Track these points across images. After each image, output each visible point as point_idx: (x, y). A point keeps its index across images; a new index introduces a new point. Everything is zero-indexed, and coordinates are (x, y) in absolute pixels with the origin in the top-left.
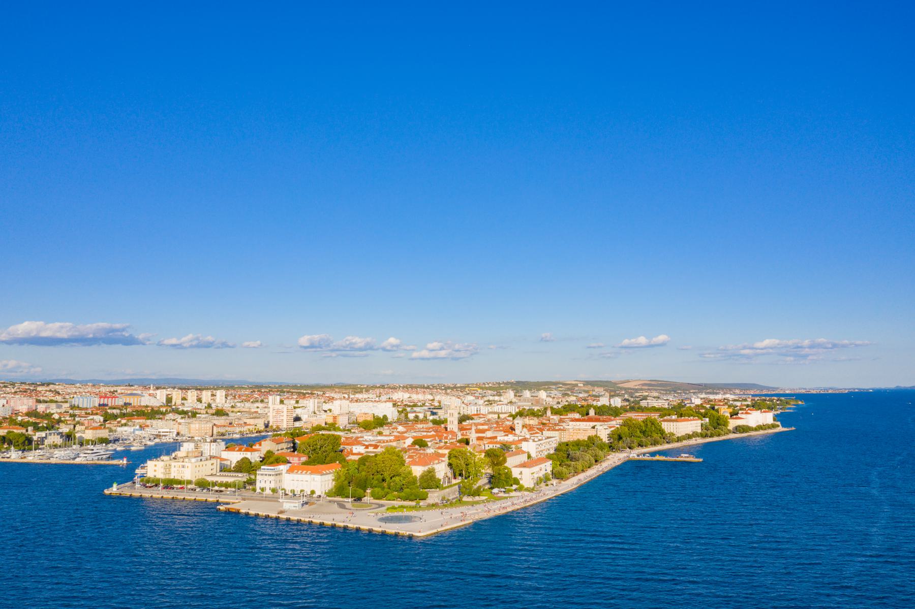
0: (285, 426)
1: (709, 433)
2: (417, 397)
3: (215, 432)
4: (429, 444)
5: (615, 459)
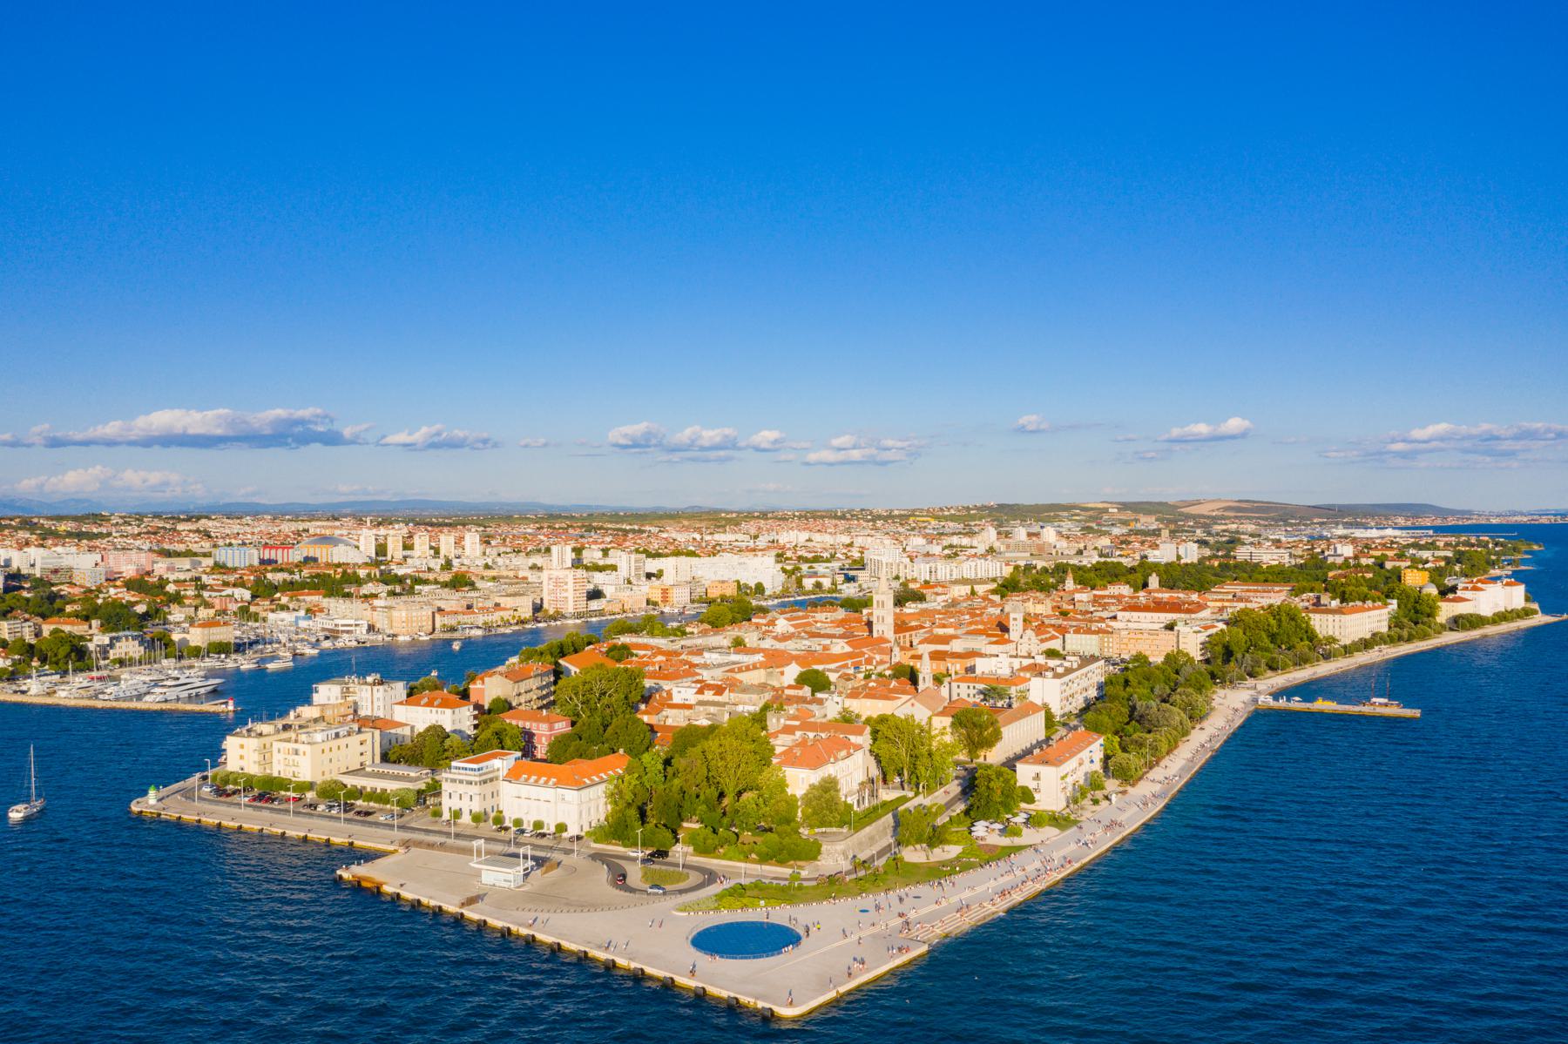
0: (571, 610)
1: (1405, 633)
2: (823, 540)
3: (438, 625)
4: (833, 677)
5: (1230, 705)
